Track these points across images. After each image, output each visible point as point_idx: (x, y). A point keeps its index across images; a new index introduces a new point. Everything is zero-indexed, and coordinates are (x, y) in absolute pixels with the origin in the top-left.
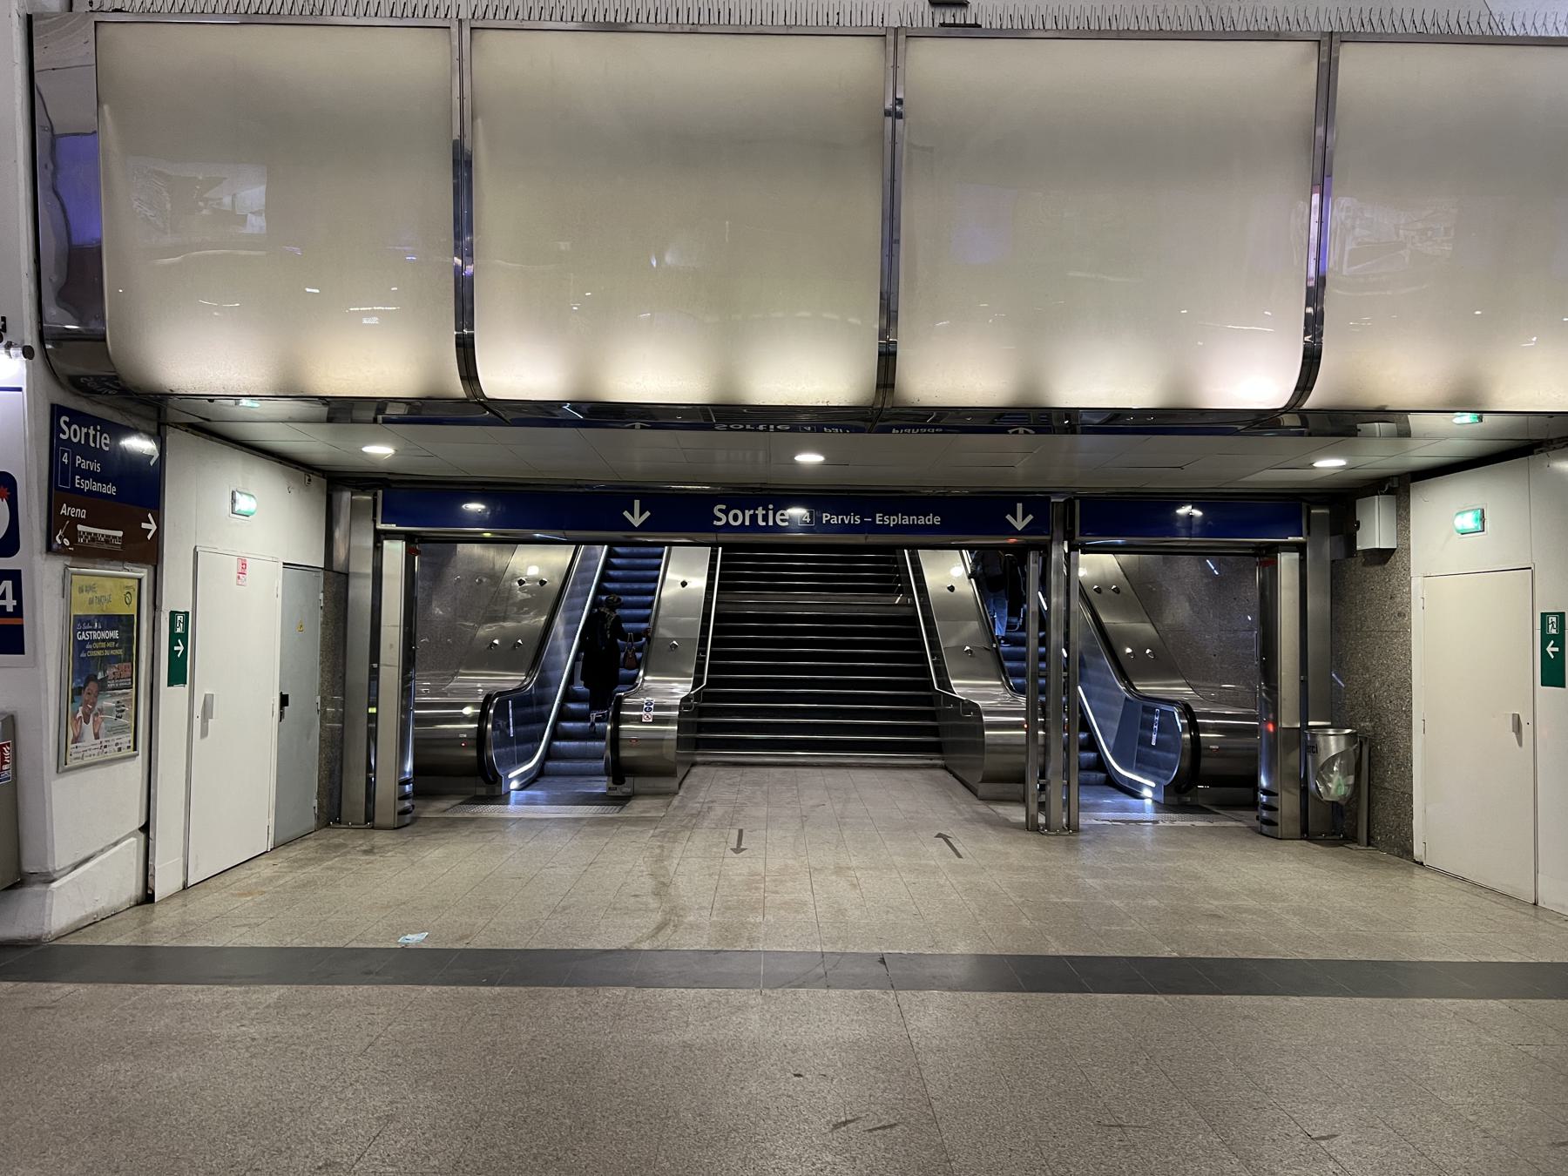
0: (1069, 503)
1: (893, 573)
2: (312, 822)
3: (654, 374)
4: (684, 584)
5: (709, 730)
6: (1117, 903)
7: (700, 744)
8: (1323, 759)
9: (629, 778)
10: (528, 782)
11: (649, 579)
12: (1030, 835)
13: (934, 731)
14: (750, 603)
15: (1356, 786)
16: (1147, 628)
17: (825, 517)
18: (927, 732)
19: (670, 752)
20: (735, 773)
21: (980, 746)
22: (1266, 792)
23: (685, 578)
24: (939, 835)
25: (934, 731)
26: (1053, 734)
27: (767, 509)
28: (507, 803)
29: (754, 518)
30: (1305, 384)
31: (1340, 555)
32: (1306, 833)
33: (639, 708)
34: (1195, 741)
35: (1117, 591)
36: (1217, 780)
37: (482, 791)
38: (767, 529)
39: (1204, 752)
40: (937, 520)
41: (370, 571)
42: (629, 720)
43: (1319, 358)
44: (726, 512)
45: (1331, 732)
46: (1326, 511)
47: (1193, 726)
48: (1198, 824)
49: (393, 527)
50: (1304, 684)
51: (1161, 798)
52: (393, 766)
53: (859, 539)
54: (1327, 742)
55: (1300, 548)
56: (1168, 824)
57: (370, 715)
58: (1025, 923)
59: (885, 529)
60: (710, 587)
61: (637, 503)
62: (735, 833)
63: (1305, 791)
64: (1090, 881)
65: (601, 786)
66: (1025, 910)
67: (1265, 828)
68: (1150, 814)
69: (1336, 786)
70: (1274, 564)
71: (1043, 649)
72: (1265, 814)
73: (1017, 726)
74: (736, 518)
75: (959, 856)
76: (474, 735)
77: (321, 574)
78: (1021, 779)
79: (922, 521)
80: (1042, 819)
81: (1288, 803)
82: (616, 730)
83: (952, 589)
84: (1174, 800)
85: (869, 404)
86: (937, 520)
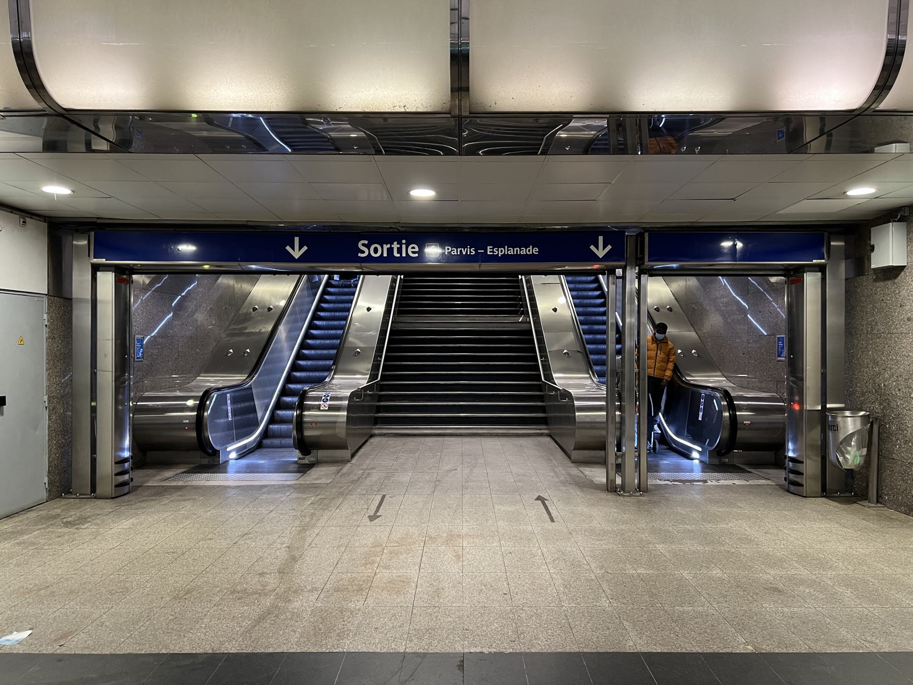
0: (640, 236)
1: (518, 301)
2: (44, 495)
3: (234, 86)
4: (369, 309)
5: (376, 412)
6: (685, 574)
7: (376, 421)
8: (842, 437)
9: (311, 449)
10: (244, 453)
11: (345, 306)
12: (611, 497)
13: (543, 409)
15: (868, 459)
16: (693, 334)
18: (535, 409)
19: (341, 432)
20: (399, 441)
22: (792, 460)
23: (370, 303)
24: (539, 498)
25: (543, 409)
26: (627, 415)
27: (401, 244)
28: (224, 471)
29: (390, 250)
30: (883, 85)
31: (851, 275)
32: (825, 492)
33: (318, 398)
34: (733, 418)
35: (670, 310)
36: (748, 446)
37: (205, 461)
38: (401, 260)
39: (739, 426)
40: (536, 251)
41: (89, 297)
42: (310, 408)
43: (902, 54)
45: (847, 413)
46: (842, 244)
47: (732, 407)
48: (737, 482)
49: (103, 261)
50: (824, 376)
51: (706, 459)
52: (115, 447)
53: (475, 267)
54: (845, 422)
55: (822, 269)
56: (714, 483)
57: (92, 407)
58: (604, 603)
59: (495, 259)
60: (387, 312)
61: (297, 239)
62: (379, 498)
63: (824, 458)
64: (660, 547)
65: (294, 456)
66: (605, 586)
67: (792, 488)
68: (697, 474)
69: (852, 457)
70: (801, 281)
71: (618, 346)
72: (792, 476)
73: (599, 409)
74: (376, 251)
76: (194, 421)
77: (45, 299)
78: (603, 447)
79: (524, 251)
80: (619, 481)
81: (811, 467)
82: (300, 417)
83: (555, 310)
84: (716, 461)
85: (447, 107)
86: (536, 251)
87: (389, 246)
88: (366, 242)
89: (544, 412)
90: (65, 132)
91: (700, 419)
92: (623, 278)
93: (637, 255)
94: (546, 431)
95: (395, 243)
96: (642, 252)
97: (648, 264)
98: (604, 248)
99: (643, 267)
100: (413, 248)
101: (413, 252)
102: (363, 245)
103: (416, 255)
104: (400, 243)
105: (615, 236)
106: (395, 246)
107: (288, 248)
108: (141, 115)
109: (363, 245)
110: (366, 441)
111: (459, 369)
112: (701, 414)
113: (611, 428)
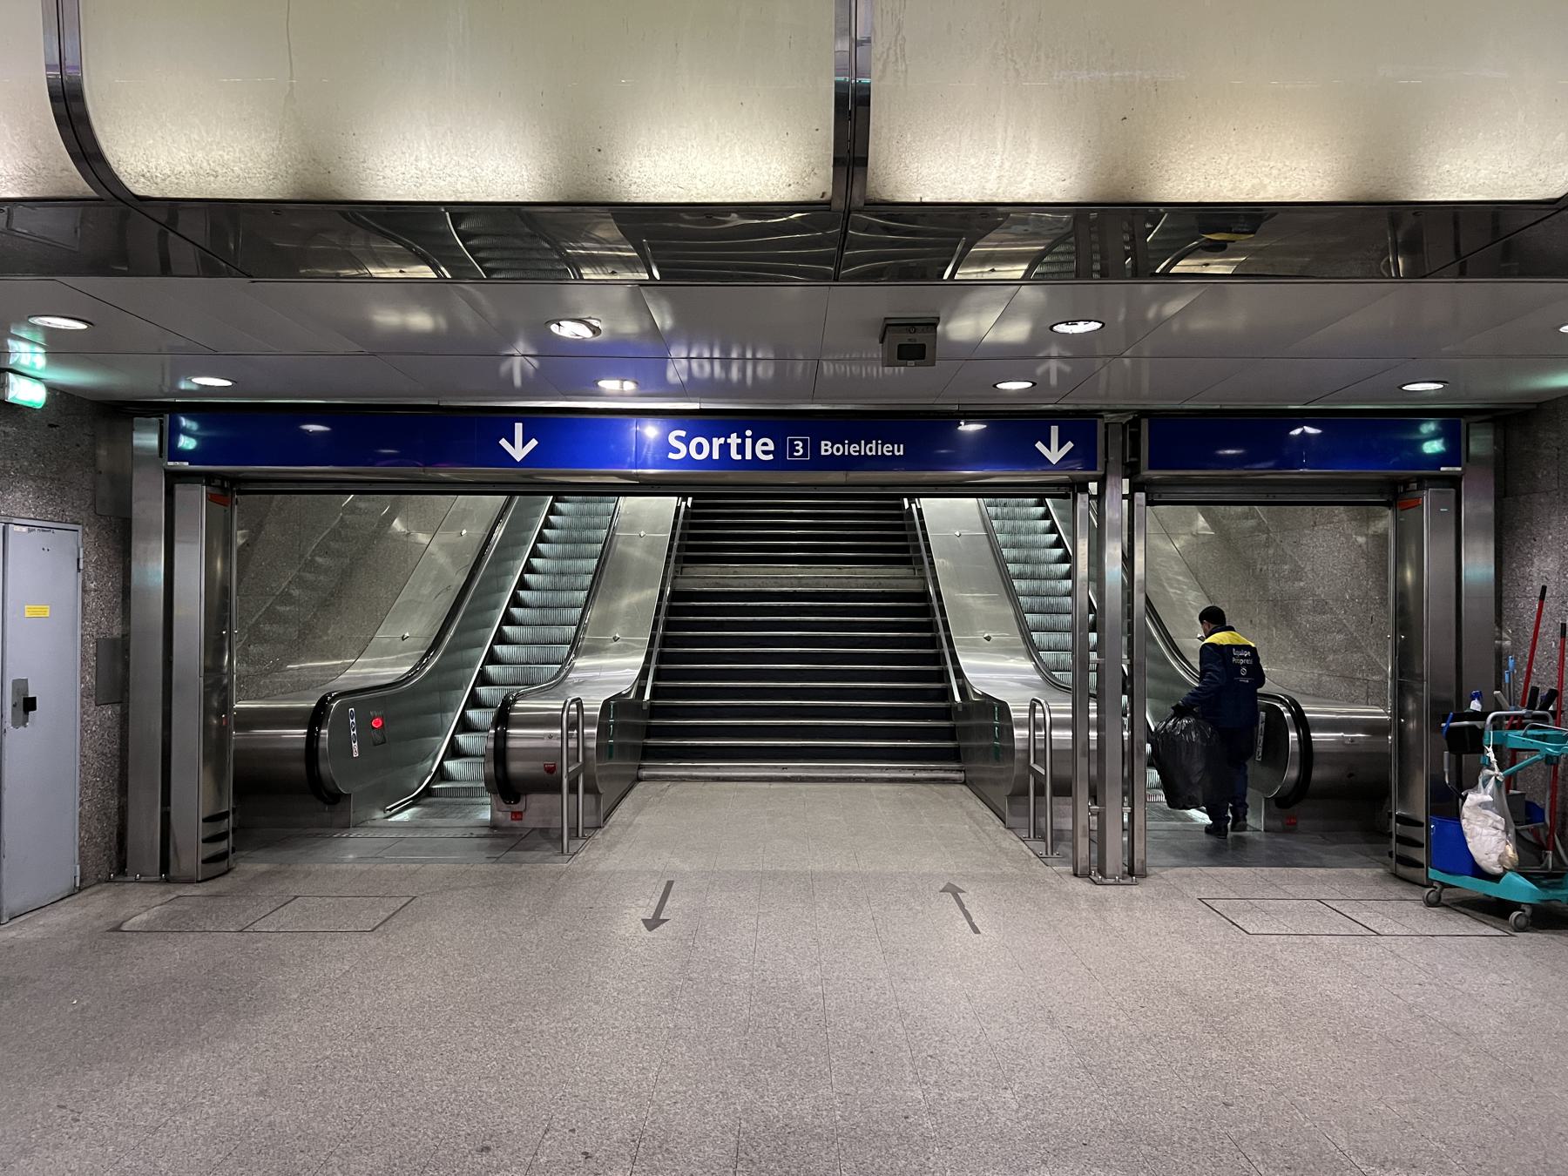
0: (1135, 423)
5: (646, 736)
7: (650, 754)
13: (950, 734)
18: (952, 737)
21: (1005, 751)
25: (950, 734)
26: (1108, 734)
27: (743, 437)
29: (725, 448)
38: (743, 464)
40: (900, 451)
52: (195, 794)
74: (700, 448)
75: (976, 931)
86: (900, 451)
87: (722, 440)
88: (683, 433)
89: (953, 739)
90: (110, 233)
91: (356, 755)
92: (1100, 497)
93: (1124, 458)
94: (960, 776)
95: (734, 435)
96: (1136, 452)
97: (1147, 474)
98: (525, 444)
99: (1139, 479)
100: (765, 444)
101: (765, 452)
102: (678, 438)
103: (771, 457)
104: (742, 436)
105: (1079, 426)
106: (734, 440)
107: (503, 442)
108: (1077, 210)
109: (678, 438)
110: (631, 788)
112: (355, 745)
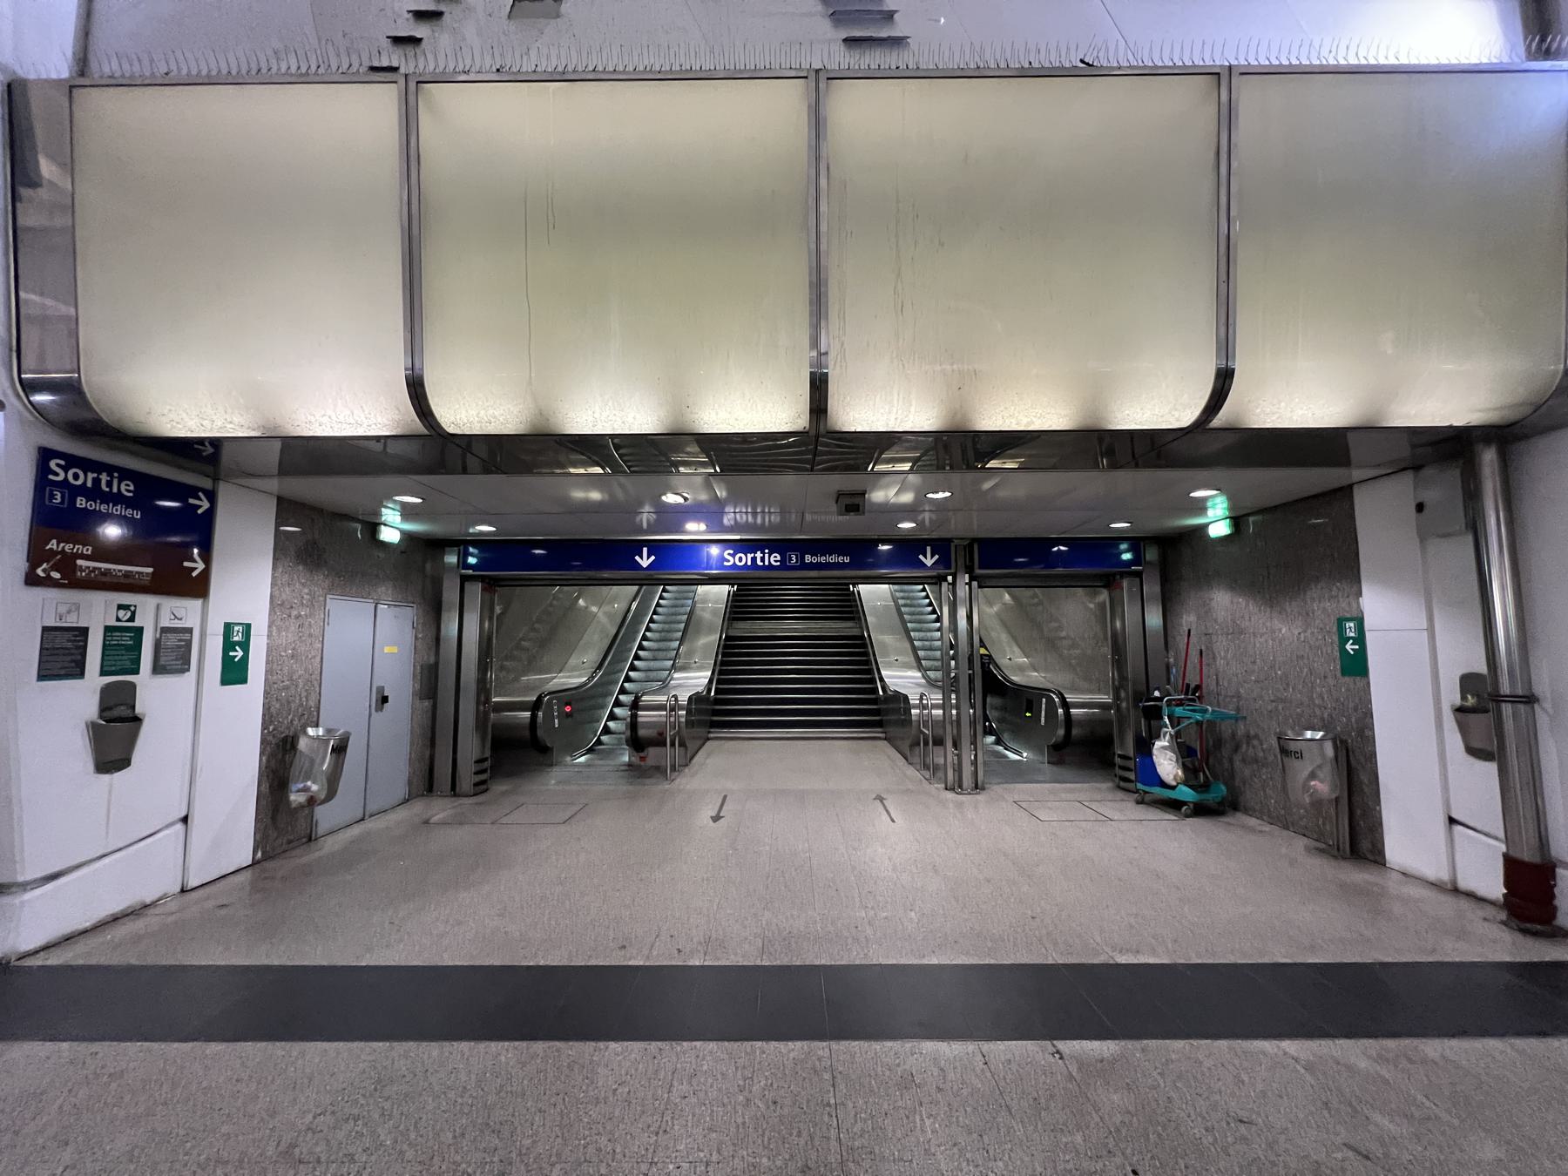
5: (713, 716)
14: (744, 628)
17: (808, 558)
18: (879, 715)
21: (907, 721)
29: (754, 559)
34: (1067, 714)
38: (764, 568)
44: (733, 555)
52: (471, 747)
79: (823, 559)
82: (634, 717)
92: (954, 584)
96: (972, 559)
97: (978, 571)
105: (941, 546)
106: (759, 555)
111: (795, 667)
113: (949, 728)
